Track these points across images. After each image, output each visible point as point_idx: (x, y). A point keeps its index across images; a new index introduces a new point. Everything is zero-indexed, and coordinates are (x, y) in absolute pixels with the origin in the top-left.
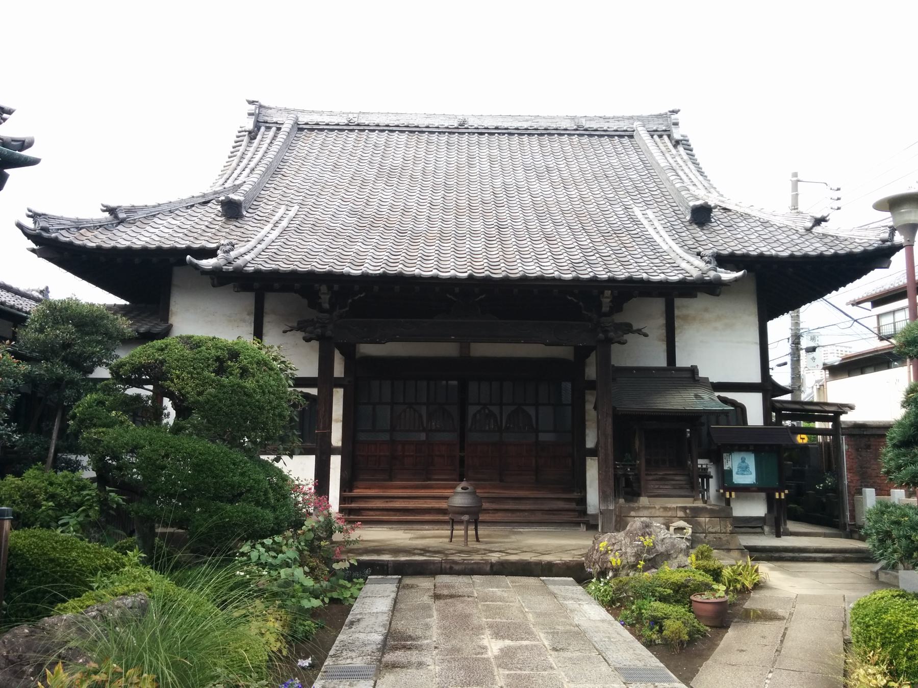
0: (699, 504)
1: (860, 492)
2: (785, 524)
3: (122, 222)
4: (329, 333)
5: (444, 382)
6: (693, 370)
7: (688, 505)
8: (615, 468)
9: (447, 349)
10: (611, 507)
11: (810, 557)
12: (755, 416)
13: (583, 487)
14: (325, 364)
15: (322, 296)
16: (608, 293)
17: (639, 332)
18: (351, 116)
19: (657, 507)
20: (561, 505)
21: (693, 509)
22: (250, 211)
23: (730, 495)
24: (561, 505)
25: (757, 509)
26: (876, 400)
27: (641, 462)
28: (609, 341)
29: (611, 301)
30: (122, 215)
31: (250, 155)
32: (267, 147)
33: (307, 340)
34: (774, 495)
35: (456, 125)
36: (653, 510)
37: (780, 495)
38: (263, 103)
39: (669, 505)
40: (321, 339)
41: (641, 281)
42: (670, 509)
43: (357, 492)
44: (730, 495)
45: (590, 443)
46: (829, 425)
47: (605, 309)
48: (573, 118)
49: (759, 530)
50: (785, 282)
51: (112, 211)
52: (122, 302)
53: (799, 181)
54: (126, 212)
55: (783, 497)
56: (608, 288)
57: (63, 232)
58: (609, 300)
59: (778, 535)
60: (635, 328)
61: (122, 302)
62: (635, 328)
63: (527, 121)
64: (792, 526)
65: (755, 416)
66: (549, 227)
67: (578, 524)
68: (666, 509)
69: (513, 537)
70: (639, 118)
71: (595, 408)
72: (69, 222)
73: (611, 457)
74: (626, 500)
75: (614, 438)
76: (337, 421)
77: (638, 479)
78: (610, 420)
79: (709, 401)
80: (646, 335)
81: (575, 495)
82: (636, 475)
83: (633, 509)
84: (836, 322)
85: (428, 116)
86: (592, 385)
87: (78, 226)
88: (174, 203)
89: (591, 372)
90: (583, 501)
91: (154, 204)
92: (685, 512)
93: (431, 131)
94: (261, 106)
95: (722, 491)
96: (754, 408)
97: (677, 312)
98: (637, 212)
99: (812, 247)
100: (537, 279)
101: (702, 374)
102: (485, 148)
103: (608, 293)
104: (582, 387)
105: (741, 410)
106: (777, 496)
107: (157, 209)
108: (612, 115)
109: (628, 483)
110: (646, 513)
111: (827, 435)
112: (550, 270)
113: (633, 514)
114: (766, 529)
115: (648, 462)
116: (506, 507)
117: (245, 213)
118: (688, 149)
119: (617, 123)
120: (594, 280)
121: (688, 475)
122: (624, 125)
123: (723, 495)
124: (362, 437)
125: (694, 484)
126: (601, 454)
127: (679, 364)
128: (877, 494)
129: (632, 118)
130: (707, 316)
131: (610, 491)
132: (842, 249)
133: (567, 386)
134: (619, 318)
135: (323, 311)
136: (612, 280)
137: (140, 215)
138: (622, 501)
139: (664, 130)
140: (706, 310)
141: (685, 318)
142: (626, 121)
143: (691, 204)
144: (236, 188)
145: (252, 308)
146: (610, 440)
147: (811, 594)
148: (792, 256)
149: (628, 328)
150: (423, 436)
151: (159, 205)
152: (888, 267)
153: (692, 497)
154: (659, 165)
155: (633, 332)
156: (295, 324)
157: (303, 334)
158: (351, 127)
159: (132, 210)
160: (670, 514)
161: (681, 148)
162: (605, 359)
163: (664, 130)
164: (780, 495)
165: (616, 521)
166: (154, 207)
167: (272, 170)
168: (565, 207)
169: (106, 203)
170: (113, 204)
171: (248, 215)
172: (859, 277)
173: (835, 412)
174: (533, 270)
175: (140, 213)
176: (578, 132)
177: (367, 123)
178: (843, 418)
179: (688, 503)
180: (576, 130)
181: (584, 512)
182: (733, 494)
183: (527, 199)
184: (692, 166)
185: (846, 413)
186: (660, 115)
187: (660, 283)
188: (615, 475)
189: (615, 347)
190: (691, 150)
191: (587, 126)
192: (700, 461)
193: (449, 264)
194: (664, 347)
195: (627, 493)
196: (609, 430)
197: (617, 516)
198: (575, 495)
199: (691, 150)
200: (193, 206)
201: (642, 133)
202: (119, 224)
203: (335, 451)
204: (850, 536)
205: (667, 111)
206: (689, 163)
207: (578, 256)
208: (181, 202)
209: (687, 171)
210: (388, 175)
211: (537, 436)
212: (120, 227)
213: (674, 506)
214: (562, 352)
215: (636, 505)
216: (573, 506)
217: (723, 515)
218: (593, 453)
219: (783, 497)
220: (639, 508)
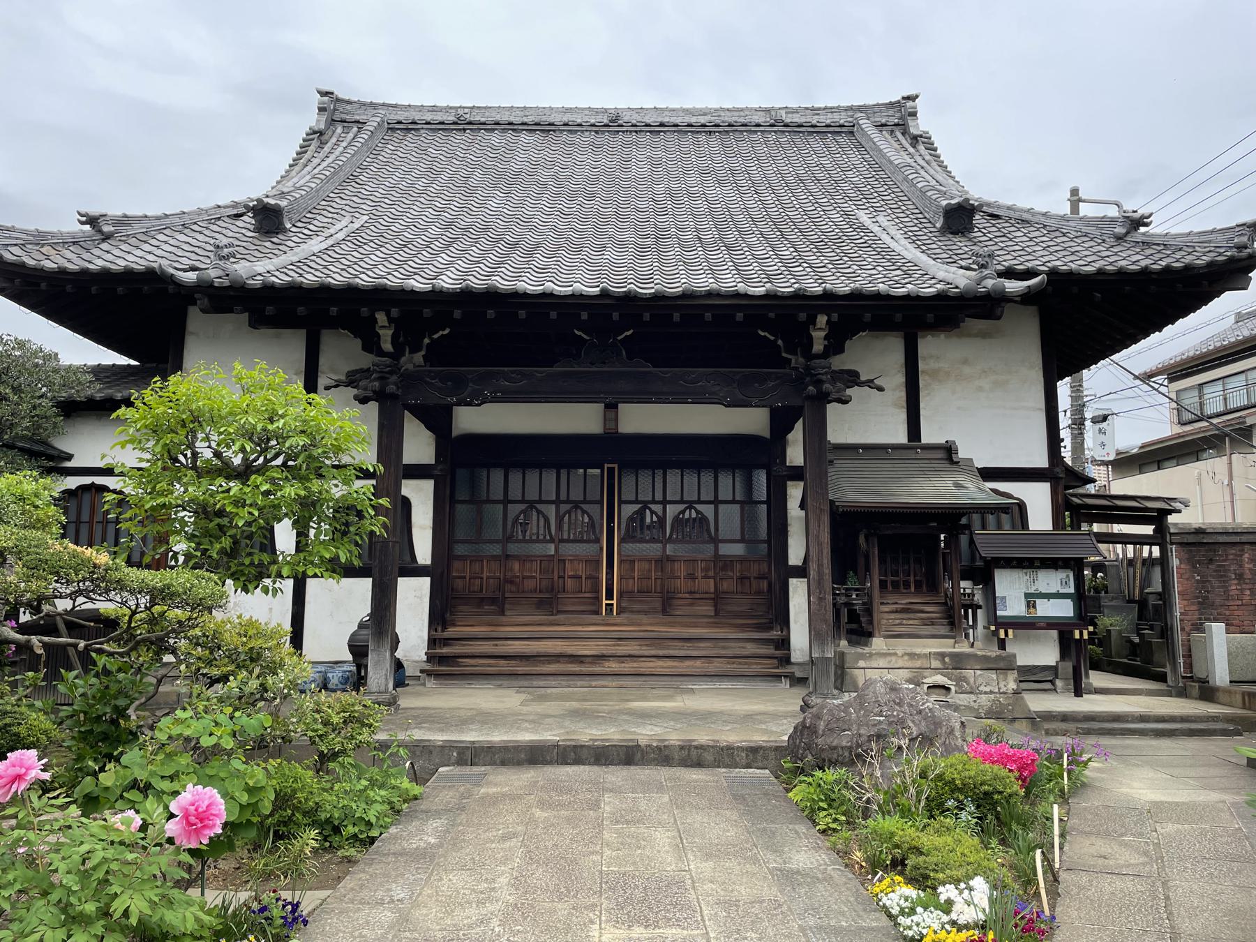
0: (963, 648)
1: (1199, 628)
2: (1087, 676)
3: (107, 237)
4: (391, 388)
5: (581, 471)
6: (948, 451)
7: (933, 650)
8: (834, 594)
9: (579, 419)
10: (830, 655)
11: (1129, 730)
12: (1040, 517)
13: (784, 621)
14: (390, 442)
15: (381, 332)
16: (822, 320)
17: (870, 383)
18: (460, 112)
19: (900, 652)
20: (751, 649)
21: (954, 656)
22: (299, 224)
23: (1006, 634)
24: (751, 649)
25: (1045, 653)
26: (1205, 496)
27: (873, 583)
28: (823, 399)
29: (826, 338)
30: (106, 229)
31: (316, 161)
32: (342, 147)
33: (363, 400)
34: (1072, 633)
35: (606, 121)
36: (894, 659)
37: (1081, 634)
38: (341, 96)
39: (918, 651)
40: (380, 396)
41: (878, 296)
42: (919, 656)
43: (452, 632)
44: (1006, 634)
45: (795, 556)
46: (1148, 530)
47: (818, 347)
48: (768, 111)
49: (1048, 686)
50: (1089, 312)
51: (92, 221)
52: (123, 360)
53: (1080, 200)
54: (113, 225)
55: (1086, 636)
56: (826, 310)
57: (13, 249)
58: (823, 334)
59: (1078, 692)
60: (863, 378)
61: (123, 360)
62: (863, 378)
63: (705, 114)
64: (1097, 679)
65: (1040, 517)
66: (732, 236)
67: (778, 677)
68: (912, 656)
69: (679, 698)
70: (860, 109)
71: (803, 506)
72: (24, 236)
73: (828, 578)
74: (850, 643)
75: (834, 550)
76: (422, 528)
77: (869, 611)
78: (826, 519)
79: (976, 493)
80: (880, 389)
81: (775, 634)
82: (864, 604)
83: (862, 657)
84: (1125, 400)
85: (568, 110)
86: (797, 474)
87: (39, 239)
88: (189, 214)
89: (795, 455)
90: (784, 643)
91: (159, 213)
92: (943, 662)
93: (572, 128)
94: (338, 100)
95: (993, 628)
96: (1038, 502)
97: (921, 366)
98: (863, 217)
99: (1130, 259)
100: (710, 294)
101: (962, 454)
102: (643, 152)
103: (822, 320)
104: (781, 477)
105: (1019, 510)
106: (1077, 636)
107: (162, 222)
108: (822, 106)
109: (853, 617)
110: (882, 663)
111: (1143, 544)
112: (729, 282)
113: (861, 663)
114: (1059, 683)
115: (883, 585)
116: (672, 652)
117: (288, 226)
118: (931, 148)
119: (830, 116)
120: (799, 296)
121: (945, 604)
122: (842, 118)
123: (995, 633)
124: (460, 550)
125: (953, 618)
126: (813, 574)
127: (926, 438)
128: (1228, 632)
129: (851, 108)
130: (967, 370)
131: (826, 627)
132: (1177, 260)
133: (761, 478)
134: (839, 362)
135: (381, 353)
136: (828, 295)
137: (137, 228)
138: (844, 643)
139: (899, 118)
140: (965, 362)
141: (934, 374)
142: (843, 113)
143: (944, 203)
144: (282, 194)
145: (302, 366)
146: (827, 551)
147: (1145, 788)
148: (1100, 272)
149: (852, 379)
150: (551, 549)
151: (167, 216)
152: (1245, 289)
153: (953, 637)
154: (891, 162)
155: (861, 384)
156: (343, 378)
157: (355, 391)
158: (463, 124)
159: (125, 220)
160: (918, 663)
161: (921, 147)
162: (817, 430)
163: (899, 118)
164: (1081, 634)
165: (836, 673)
166: (158, 218)
167: (342, 176)
168: (755, 215)
169: (83, 211)
170: (94, 211)
171: (294, 229)
172: (1184, 315)
173: (1156, 514)
174: (703, 282)
175: (136, 226)
176: (775, 129)
177: (483, 120)
178: (1172, 519)
179: (946, 646)
180: (772, 125)
181: (786, 660)
182: (1010, 632)
183: (701, 205)
184: (938, 169)
185: (1179, 511)
186: (891, 104)
187: (907, 297)
188: (834, 605)
189: (833, 410)
190: (935, 150)
191: (788, 120)
192: (963, 584)
193: (576, 278)
194: (903, 416)
195: (850, 632)
196: (825, 537)
197: (836, 666)
198: (775, 634)
199: (935, 150)
200: (219, 219)
201: (866, 125)
202: (103, 240)
203: (414, 570)
204: (1182, 693)
205: (899, 98)
206: (934, 164)
207: (774, 266)
208: (200, 211)
209: (932, 172)
210: (506, 181)
211: (716, 549)
212: (105, 246)
213: (927, 651)
214: (750, 420)
215: (867, 650)
216: (770, 650)
217: (1002, 665)
218: (801, 572)
219: (1086, 636)
220: (871, 655)
